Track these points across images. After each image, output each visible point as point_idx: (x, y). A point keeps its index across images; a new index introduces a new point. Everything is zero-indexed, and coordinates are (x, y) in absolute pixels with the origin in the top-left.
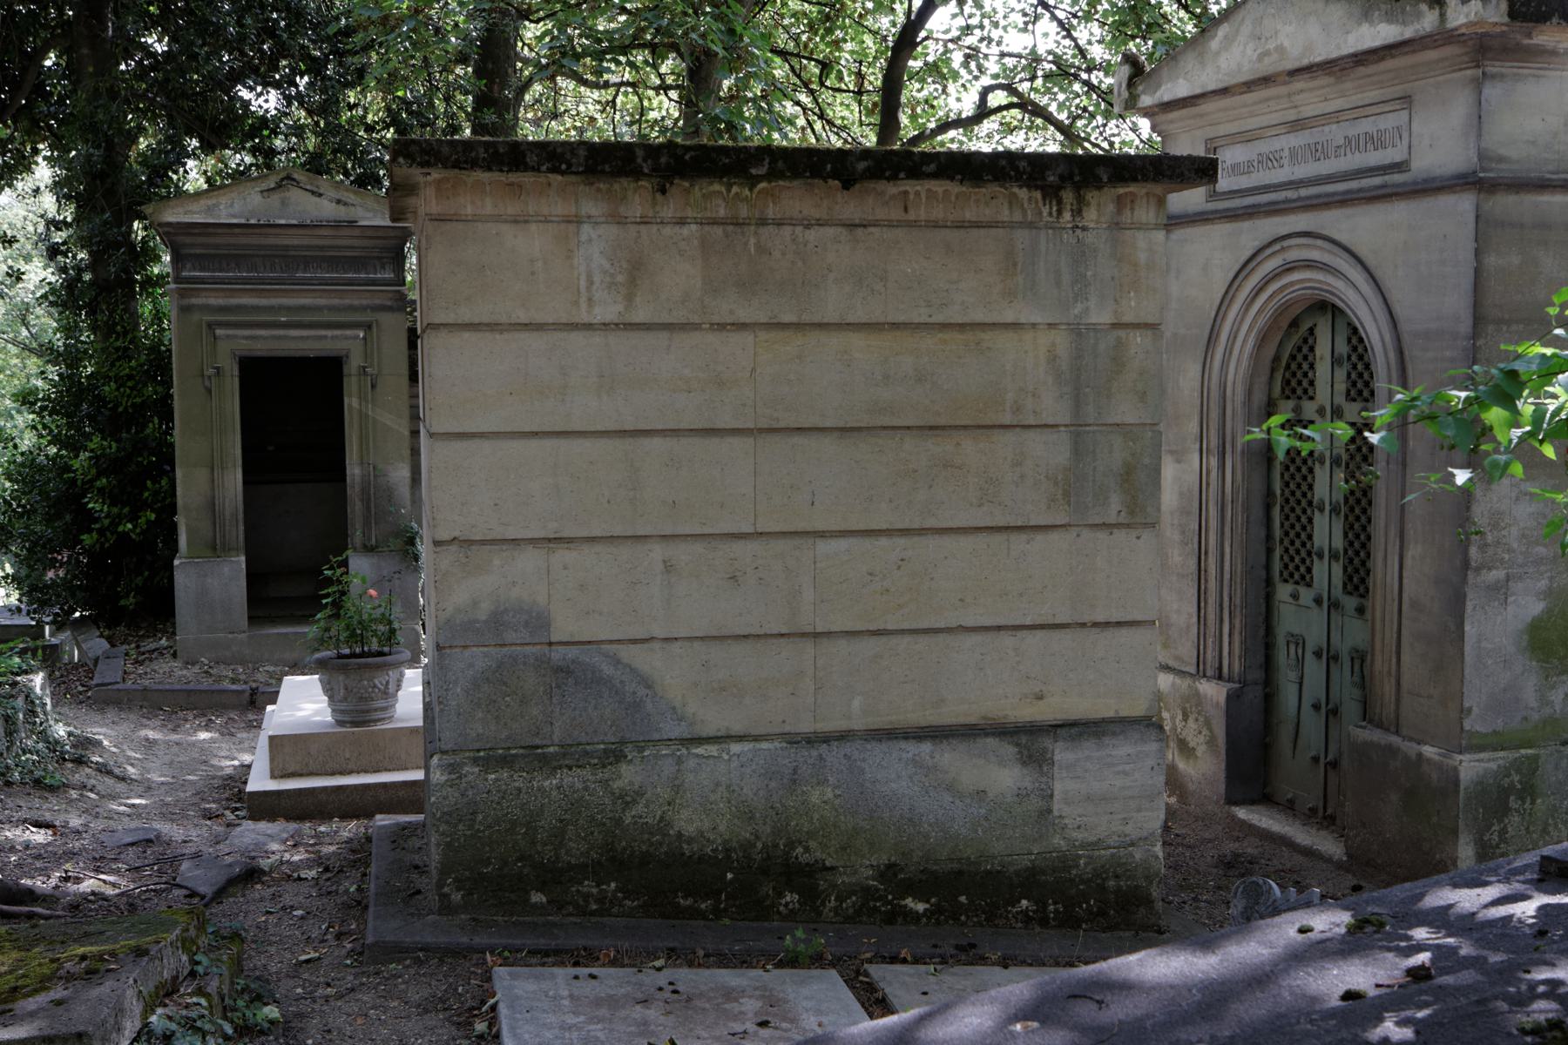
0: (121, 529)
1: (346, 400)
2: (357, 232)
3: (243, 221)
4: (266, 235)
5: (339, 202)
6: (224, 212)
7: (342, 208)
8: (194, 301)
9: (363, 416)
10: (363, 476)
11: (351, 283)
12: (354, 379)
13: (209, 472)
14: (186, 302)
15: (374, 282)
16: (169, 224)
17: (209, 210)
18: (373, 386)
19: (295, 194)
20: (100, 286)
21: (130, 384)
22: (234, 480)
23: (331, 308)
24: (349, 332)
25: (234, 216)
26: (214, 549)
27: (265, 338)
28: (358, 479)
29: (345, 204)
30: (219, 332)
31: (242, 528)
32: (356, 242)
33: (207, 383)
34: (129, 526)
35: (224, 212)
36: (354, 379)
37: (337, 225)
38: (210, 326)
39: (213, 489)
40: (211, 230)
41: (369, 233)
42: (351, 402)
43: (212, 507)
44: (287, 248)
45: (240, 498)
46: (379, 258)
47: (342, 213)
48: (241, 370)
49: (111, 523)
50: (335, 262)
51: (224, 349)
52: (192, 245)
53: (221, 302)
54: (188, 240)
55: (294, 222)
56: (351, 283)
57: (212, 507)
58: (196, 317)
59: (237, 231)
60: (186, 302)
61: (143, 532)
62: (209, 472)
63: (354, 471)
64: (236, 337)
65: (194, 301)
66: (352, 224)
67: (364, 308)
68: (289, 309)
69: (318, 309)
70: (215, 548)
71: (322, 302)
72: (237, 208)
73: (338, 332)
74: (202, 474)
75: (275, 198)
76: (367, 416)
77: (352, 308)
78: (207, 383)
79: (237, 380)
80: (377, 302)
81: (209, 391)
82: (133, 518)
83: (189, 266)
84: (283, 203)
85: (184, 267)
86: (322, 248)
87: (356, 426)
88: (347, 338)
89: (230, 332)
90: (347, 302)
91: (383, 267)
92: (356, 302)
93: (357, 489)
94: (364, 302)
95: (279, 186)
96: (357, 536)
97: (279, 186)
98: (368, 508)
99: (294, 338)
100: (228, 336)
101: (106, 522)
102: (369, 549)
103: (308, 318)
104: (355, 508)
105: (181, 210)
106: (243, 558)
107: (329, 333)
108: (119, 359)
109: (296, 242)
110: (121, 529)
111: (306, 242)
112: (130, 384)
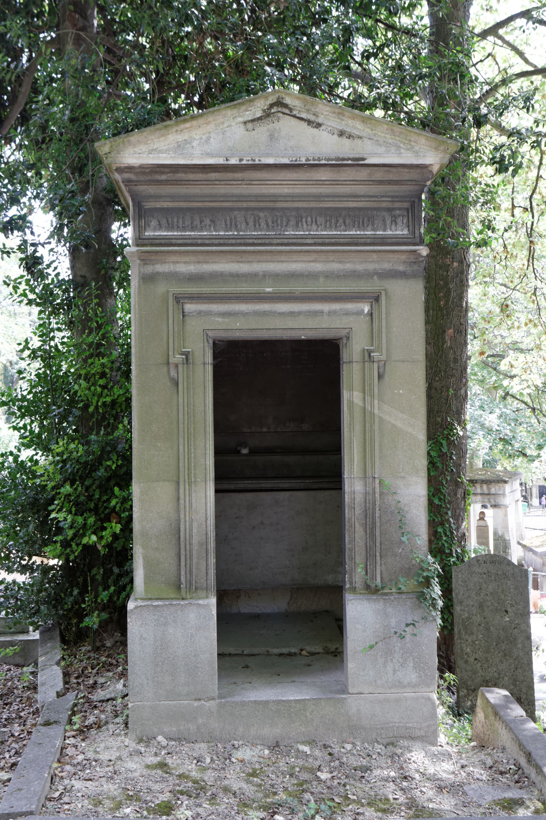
0: (85, 541)
1: (345, 395)
2: (363, 174)
3: (221, 161)
4: (250, 182)
5: (341, 134)
6: (197, 151)
7: (345, 141)
8: (160, 268)
9: (367, 416)
10: (366, 494)
11: (354, 242)
12: (356, 368)
13: (174, 494)
14: (149, 269)
15: (383, 241)
16: (130, 169)
17: (179, 147)
18: (380, 377)
19: (286, 125)
20: (86, 296)
21: (102, 382)
22: (204, 498)
23: (328, 276)
24: (350, 306)
25: (210, 155)
26: (179, 588)
27: (245, 314)
28: (359, 498)
29: (350, 137)
30: (189, 307)
31: (212, 560)
32: (361, 189)
33: (173, 373)
34: (94, 538)
35: (197, 151)
36: (356, 368)
37: (339, 165)
38: (179, 299)
39: (178, 511)
40: (181, 176)
41: (379, 175)
42: (351, 397)
43: (176, 533)
44: (275, 198)
45: (211, 521)
46: (389, 210)
47: (345, 148)
48: (215, 357)
49: (75, 535)
50: (334, 216)
51: (195, 327)
52: (158, 197)
53: (192, 268)
54: (152, 190)
55: (286, 161)
56: (354, 242)
57: (176, 533)
58: (161, 288)
59: (213, 176)
60: (149, 269)
61: (109, 546)
62: (174, 494)
63: (353, 485)
64: (209, 313)
65: (160, 268)
66: (358, 163)
67: (368, 275)
68: (276, 277)
69: (312, 276)
70: (180, 587)
71: (318, 267)
72: (215, 144)
73: (336, 306)
74: (164, 491)
75: (262, 131)
76: (372, 414)
77: (354, 275)
78: (173, 373)
79: (210, 369)
80: (386, 266)
81: (176, 384)
82: (99, 530)
83: (154, 223)
84: (272, 137)
85: (147, 225)
86: (318, 197)
87: (358, 428)
88: (347, 313)
89: (203, 307)
90: (349, 266)
91: (394, 221)
92: (360, 267)
93: (358, 511)
94: (371, 267)
95: (267, 115)
96: (356, 573)
97: (267, 115)
98: (373, 536)
99: (282, 314)
100: (200, 313)
101: (70, 533)
102: (371, 590)
103: (298, 288)
104: (355, 536)
105: (143, 148)
106: (213, 601)
107: (326, 307)
108: (91, 356)
109: (286, 190)
110: (85, 541)
111: (298, 190)
112: (102, 382)
